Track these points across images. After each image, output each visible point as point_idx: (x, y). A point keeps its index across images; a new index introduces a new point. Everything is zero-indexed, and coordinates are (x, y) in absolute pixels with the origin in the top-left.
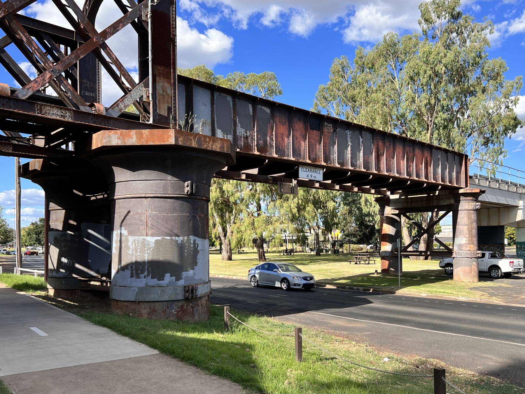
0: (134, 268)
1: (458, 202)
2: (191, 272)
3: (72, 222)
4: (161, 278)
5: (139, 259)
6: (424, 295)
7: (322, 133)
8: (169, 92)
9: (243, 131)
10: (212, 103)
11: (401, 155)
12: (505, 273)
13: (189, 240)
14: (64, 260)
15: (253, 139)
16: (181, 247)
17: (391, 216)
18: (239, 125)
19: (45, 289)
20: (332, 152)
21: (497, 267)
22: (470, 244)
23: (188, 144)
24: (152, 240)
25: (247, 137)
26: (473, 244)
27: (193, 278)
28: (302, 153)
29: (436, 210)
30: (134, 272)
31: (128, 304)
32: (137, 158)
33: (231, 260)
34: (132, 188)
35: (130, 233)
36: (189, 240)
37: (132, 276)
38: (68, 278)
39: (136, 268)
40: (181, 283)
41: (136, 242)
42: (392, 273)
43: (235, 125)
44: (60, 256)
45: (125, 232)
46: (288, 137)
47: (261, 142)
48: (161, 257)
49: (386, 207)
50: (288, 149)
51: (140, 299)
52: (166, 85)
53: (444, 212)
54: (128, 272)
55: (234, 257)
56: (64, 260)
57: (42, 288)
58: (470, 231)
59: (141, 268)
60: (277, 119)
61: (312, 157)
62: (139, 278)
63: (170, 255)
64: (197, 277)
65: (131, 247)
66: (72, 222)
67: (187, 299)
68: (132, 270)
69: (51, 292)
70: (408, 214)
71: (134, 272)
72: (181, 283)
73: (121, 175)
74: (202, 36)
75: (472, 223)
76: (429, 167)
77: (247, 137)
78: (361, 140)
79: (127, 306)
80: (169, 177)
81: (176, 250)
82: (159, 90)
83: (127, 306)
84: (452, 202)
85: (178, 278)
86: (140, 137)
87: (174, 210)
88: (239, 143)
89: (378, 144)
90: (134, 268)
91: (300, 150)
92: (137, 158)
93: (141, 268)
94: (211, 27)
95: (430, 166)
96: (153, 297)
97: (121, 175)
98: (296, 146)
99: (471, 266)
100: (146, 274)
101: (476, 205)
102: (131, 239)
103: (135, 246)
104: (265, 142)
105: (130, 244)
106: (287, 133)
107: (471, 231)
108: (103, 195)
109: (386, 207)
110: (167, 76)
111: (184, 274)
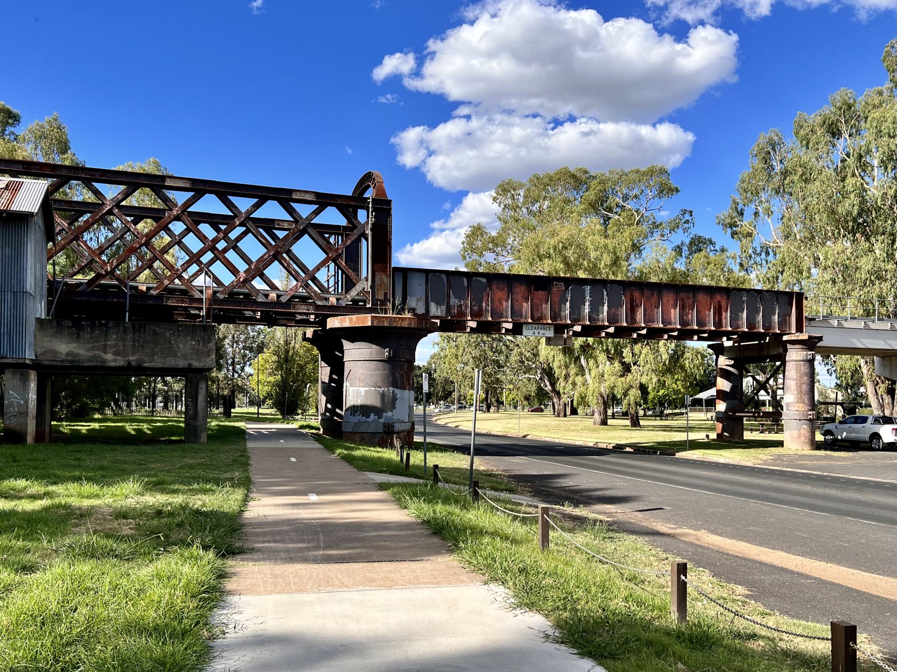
1: (786, 350)
2: (390, 414)
3: (334, 376)
4: (368, 417)
5: (355, 404)
6: (721, 460)
7: (550, 293)
8: (385, 281)
9: (456, 301)
10: (427, 283)
11: (671, 302)
12: (889, 444)
13: (388, 390)
15: (466, 306)
16: (383, 395)
17: (725, 367)
18: (452, 296)
19: (319, 429)
20: (563, 309)
21: (876, 436)
22: (798, 402)
23: (381, 325)
24: (363, 390)
25: (461, 306)
26: (804, 403)
27: (391, 418)
28: (524, 314)
32: (356, 334)
33: (606, 424)
34: (356, 355)
35: (351, 385)
36: (388, 390)
38: (331, 419)
39: (354, 409)
40: (382, 420)
42: (725, 439)
43: (449, 297)
44: (327, 403)
45: (348, 384)
46: (507, 301)
47: (476, 308)
48: (368, 402)
50: (507, 311)
51: (355, 430)
52: (383, 276)
54: (349, 412)
55: (610, 422)
56: (329, 406)
57: (318, 429)
58: (799, 387)
60: (494, 287)
61: (536, 316)
63: (375, 401)
64: (395, 418)
66: (334, 376)
67: (385, 432)
69: (321, 432)
72: (382, 420)
73: (346, 345)
74: (679, 47)
75: (801, 377)
76: (724, 314)
77: (461, 306)
78: (605, 293)
80: (374, 346)
81: (379, 397)
82: (377, 281)
84: (781, 350)
85: (380, 417)
86: (351, 320)
87: (378, 369)
88: (452, 311)
89: (632, 296)
91: (521, 311)
92: (356, 334)
94: (702, 23)
95: (726, 311)
96: (363, 429)
97: (346, 345)
98: (517, 308)
99: (800, 430)
101: (807, 355)
102: (351, 389)
104: (480, 308)
106: (506, 297)
107: (801, 387)
110: (384, 270)
111: (384, 414)
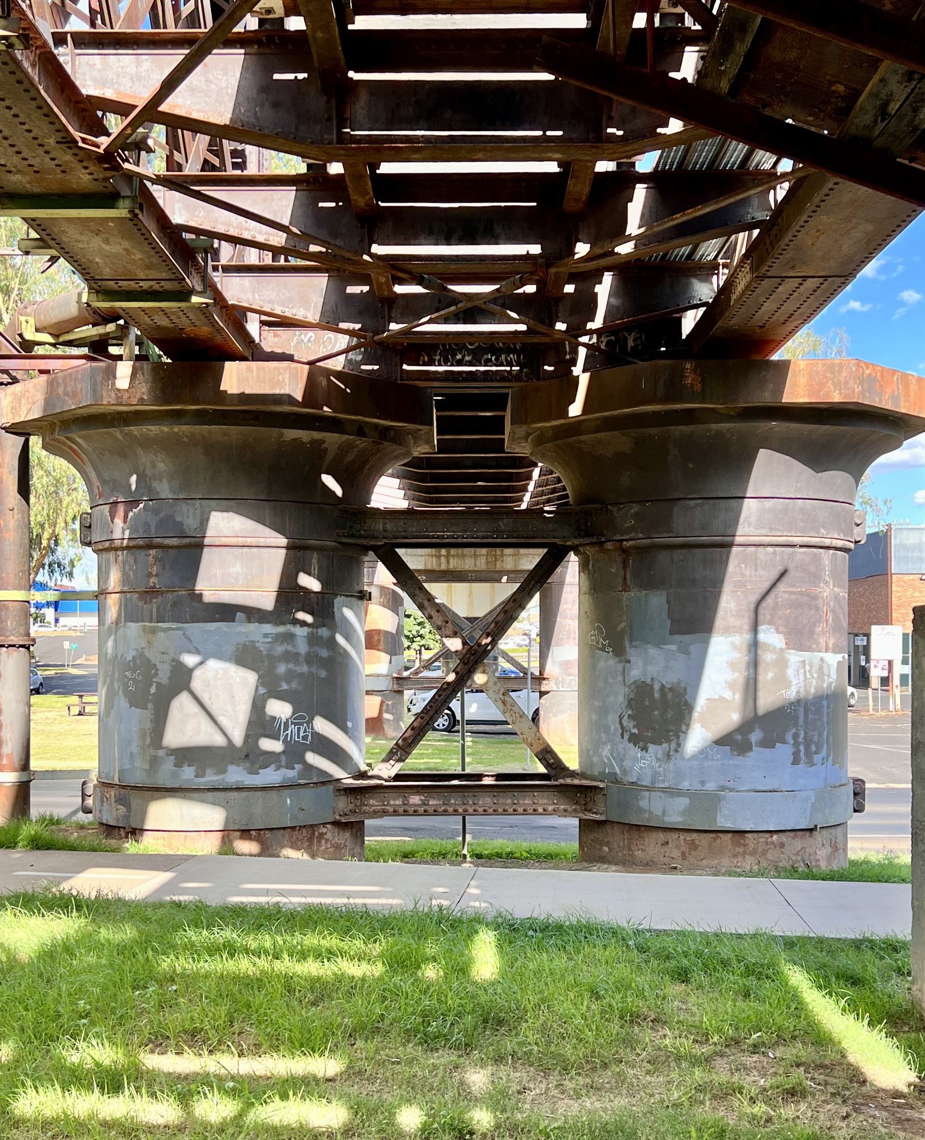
0: (801, 739)
14: (280, 709)
29: (348, 391)
30: (802, 748)
31: (783, 838)
37: (796, 761)
41: (807, 668)
49: (585, 15)
53: (187, 236)
56: (280, 709)
59: (816, 738)
62: (813, 765)
65: (794, 682)
68: (796, 744)
70: (756, 232)
71: (802, 748)
79: (782, 845)
83: (782, 845)
90: (801, 739)
93: (816, 738)
100: (824, 753)
102: (794, 657)
103: (806, 679)
105: (790, 672)
108: (327, 249)
109: (585, 15)
